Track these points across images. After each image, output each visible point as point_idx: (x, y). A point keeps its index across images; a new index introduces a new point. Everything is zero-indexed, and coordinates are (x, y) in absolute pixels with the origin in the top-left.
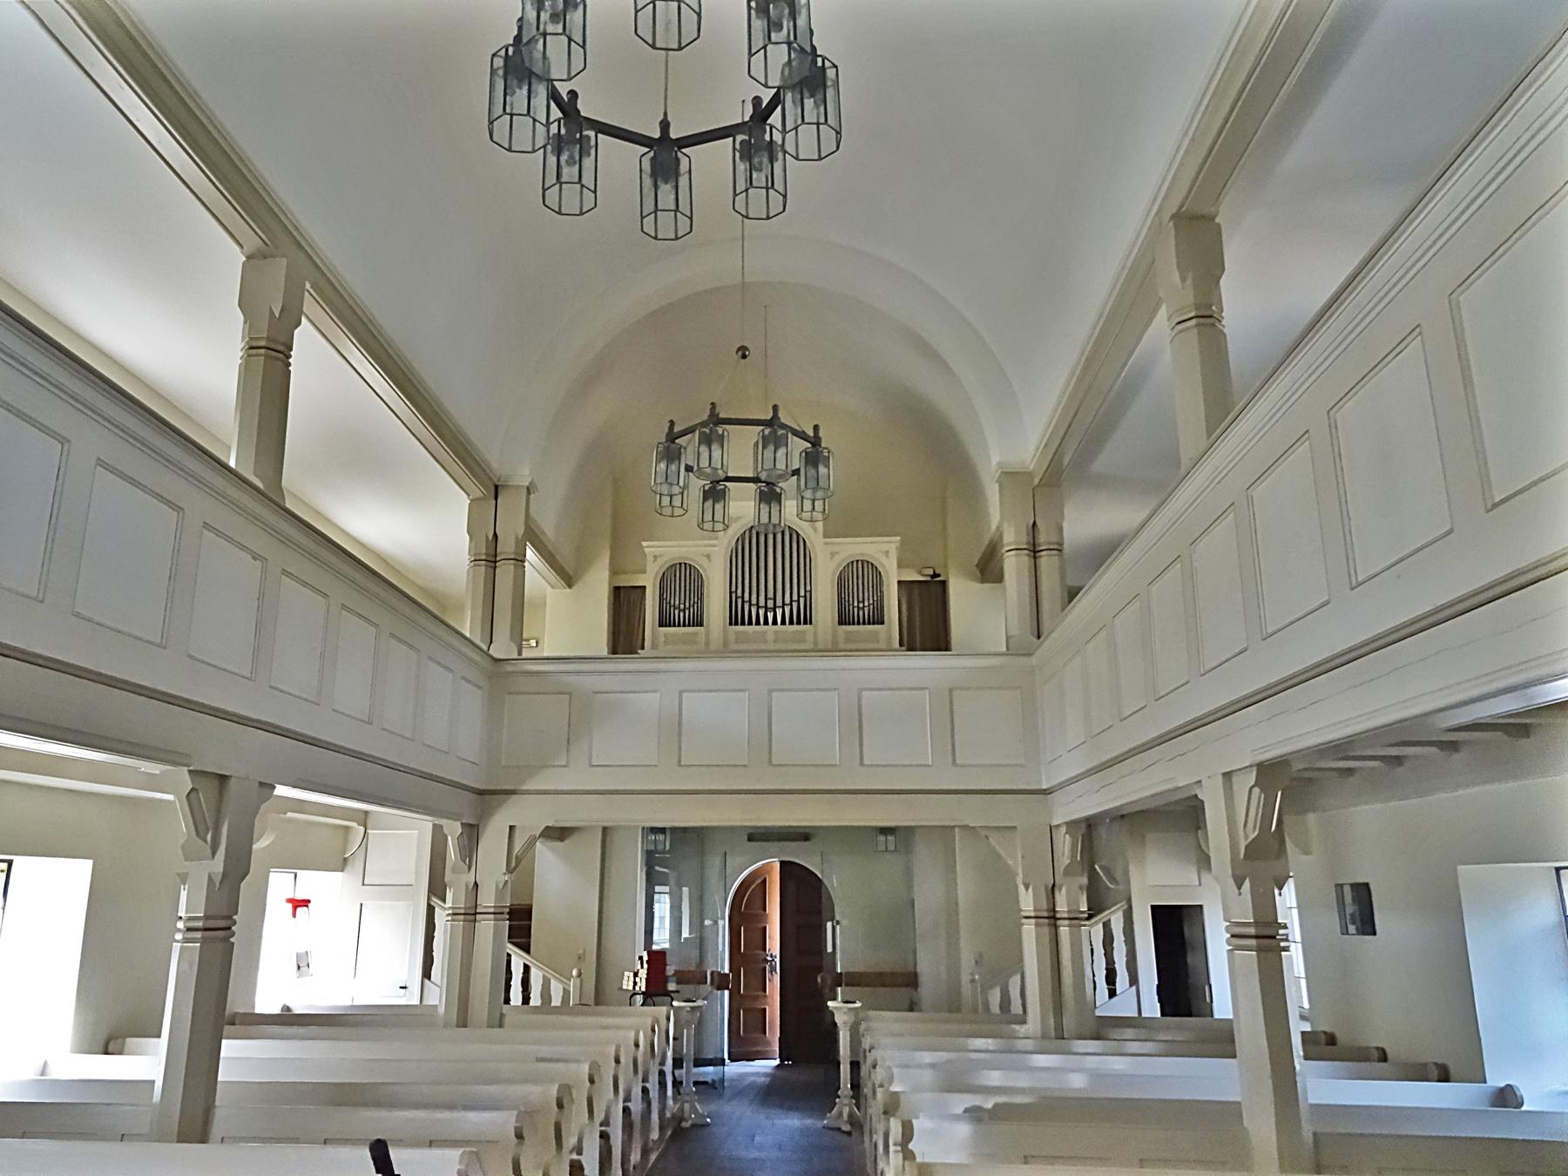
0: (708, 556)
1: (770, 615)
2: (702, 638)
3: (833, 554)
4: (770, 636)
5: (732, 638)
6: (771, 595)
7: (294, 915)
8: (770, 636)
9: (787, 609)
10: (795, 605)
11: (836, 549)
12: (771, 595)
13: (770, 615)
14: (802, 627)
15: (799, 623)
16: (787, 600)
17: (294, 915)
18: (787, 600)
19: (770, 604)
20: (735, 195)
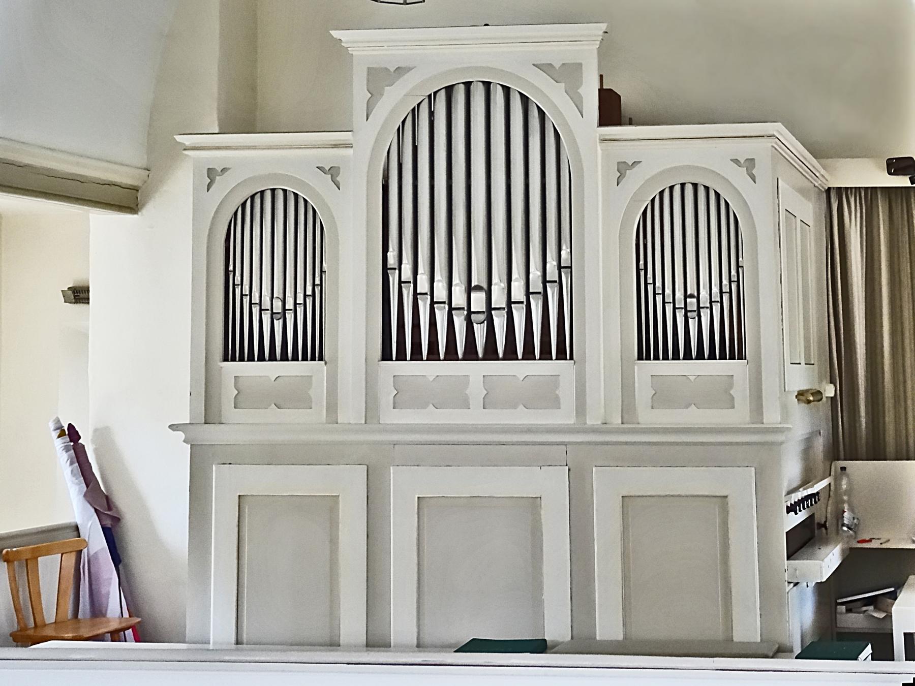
0: (333, 172)
1: (480, 332)
2: (319, 391)
3: (623, 169)
4: (476, 391)
5: (387, 394)
6: (278, 292)
7: (173, 427)
8: (476, 391)
9: (500, 323)
10: (716, 308)
11: (627, 153)
12: (278, 292)
13: (480, 332)
14: (552, 366)
15: (546, 354)
16: (518, 293)
17: (173, 427)
18: (518, 293)
19: (478, 301)
20: (321, 285)
